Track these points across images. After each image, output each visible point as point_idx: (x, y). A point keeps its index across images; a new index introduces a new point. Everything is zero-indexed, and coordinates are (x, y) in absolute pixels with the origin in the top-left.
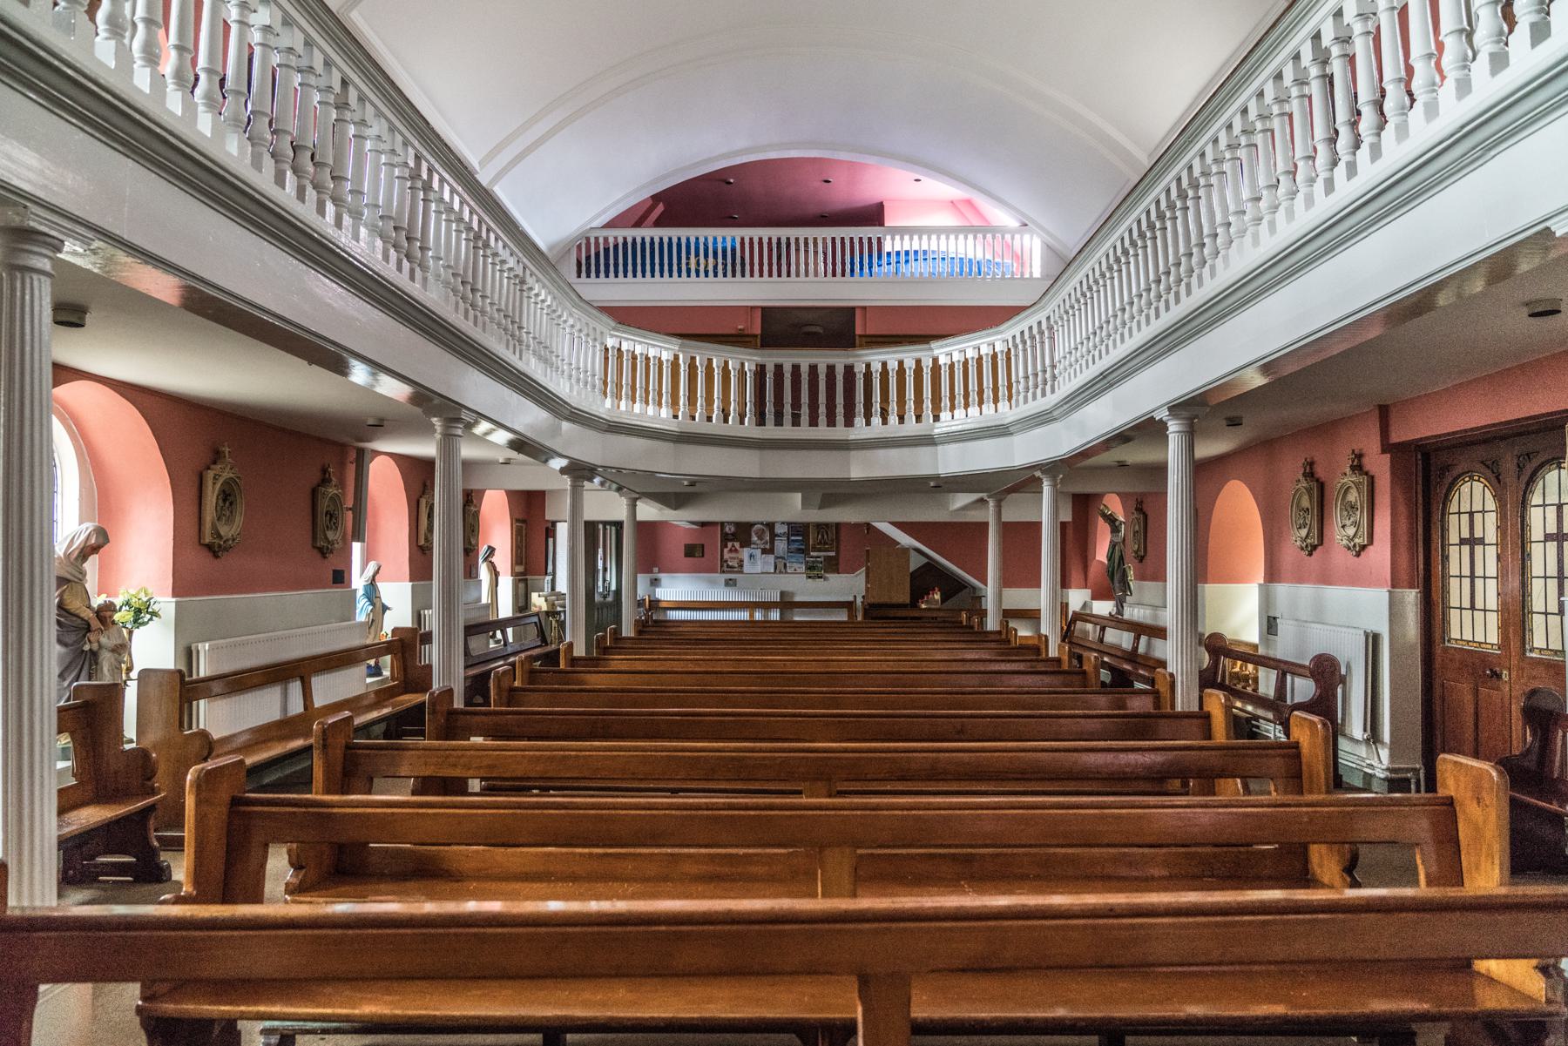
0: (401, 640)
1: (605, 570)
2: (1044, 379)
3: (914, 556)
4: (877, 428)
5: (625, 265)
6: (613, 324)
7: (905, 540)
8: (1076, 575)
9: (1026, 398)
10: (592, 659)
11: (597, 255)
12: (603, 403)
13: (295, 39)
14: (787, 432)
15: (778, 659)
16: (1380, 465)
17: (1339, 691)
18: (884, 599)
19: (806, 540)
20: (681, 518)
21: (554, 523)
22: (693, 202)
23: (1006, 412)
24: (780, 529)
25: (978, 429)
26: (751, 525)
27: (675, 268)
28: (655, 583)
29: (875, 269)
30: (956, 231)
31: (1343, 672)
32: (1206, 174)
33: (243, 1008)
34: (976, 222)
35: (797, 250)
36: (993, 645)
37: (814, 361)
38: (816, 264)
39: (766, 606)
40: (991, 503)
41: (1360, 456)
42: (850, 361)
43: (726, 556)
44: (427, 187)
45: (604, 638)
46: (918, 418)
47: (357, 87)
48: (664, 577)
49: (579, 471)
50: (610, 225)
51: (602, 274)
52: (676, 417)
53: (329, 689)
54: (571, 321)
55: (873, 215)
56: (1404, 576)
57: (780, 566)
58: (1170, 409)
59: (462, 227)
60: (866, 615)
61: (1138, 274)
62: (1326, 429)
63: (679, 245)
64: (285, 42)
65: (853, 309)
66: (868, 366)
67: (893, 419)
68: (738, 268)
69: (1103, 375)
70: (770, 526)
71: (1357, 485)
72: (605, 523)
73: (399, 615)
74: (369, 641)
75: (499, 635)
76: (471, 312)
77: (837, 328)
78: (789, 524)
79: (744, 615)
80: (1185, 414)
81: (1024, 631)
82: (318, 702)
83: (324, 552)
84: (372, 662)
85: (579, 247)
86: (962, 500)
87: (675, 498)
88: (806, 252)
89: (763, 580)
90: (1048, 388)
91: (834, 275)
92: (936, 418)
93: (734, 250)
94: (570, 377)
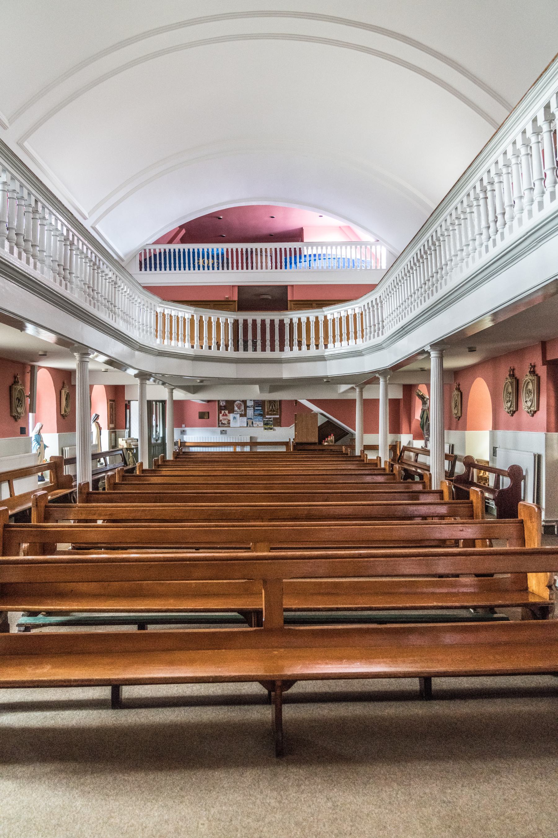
0: (54, 462)
1: (157, 426)
2: (380, 327)
3: (320, 416)
4: (296, 353)
5: (165, 264)
6: (160, 300)
7: (315, 409)
8: (404, 426)
9: (370, 337)
10: (152, 470)
11: (150, 258)
12: (156, 341)
13: (16, 186)
14: (250, 354)
15: (245, 469)
16: (542, 371)
17: (522, 483)
18: (305, 440)
19: (263, 409)
20: (197, 398)
21: (129, 402)
22: (200, 230)
23: (361, 344)
24: (249, 404)
25: (349, 351)
26: (235, 401)
27: (192, 265)
28: (183, 432)
29: (298, 264)
30: (342, 244)
31: (524, 473)
32: (442, 235)
33: (17, 607)
34: (354, 239)
35: (257, 255)
36: (357, 462)
37: (263, 317)
38: (266, 262)
39: (243, 444)
40: (358, 390)
41: (534, 367)
42: (282, 317)
43: (221, 418)
44: (72, 244)
45: (158, 460)
46: (317, 346)
47: (42, 203)
48: (188, 429)
49: (143, 376)
50: (157, 242)
51: (153, 269)
52: (193, 347)
53: (22, 486)
54: (139, 301)
55: (297, 235)
56: (553, 425)
57: (250, 423)
58: (431, 346)
59: (87, 261)
60: (294, 449)
61: (417, 280)
62: (519, 353)
63: (194, 253)
64: (11, 188)
65: (286, 287)
66: (291, 320)
67: (304, 347)
68: (225, 265)
69: (403, 328)
70: (244, 402)
71: (532, 381)
72: (156, 401)
73: (52, 450)
74: (39, 463)
75: (102, 460)
76: (92, 301)
77: (276, 299)
78: (254, 401)
79: (231, 449)
80: (438, 348)
81: (371, 456)
82: (17, 493)
83: (16, 418)
84: (40, 474)
85: (141, 254)
86: (343, 388)
87: (195, 387)
88: (261, 255)
89: (242, 430)
90: (380, 332)
91: (276, 268)
92: (326, 347)
93: (223, 254)
94: (139, 329)
